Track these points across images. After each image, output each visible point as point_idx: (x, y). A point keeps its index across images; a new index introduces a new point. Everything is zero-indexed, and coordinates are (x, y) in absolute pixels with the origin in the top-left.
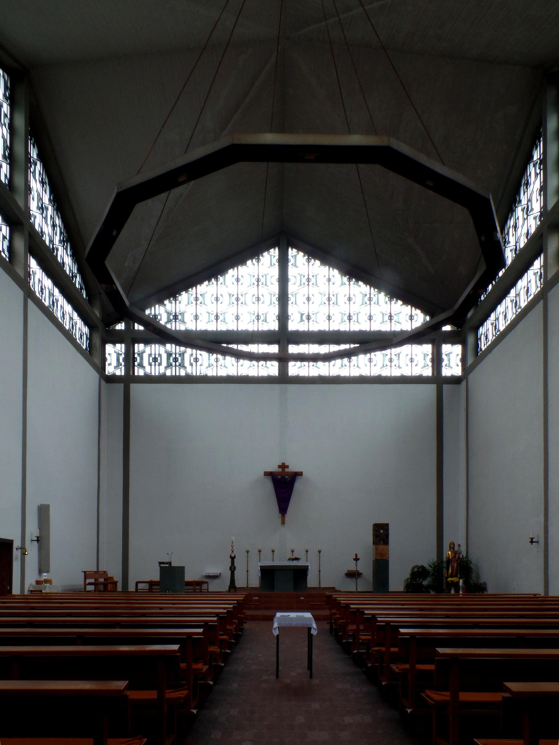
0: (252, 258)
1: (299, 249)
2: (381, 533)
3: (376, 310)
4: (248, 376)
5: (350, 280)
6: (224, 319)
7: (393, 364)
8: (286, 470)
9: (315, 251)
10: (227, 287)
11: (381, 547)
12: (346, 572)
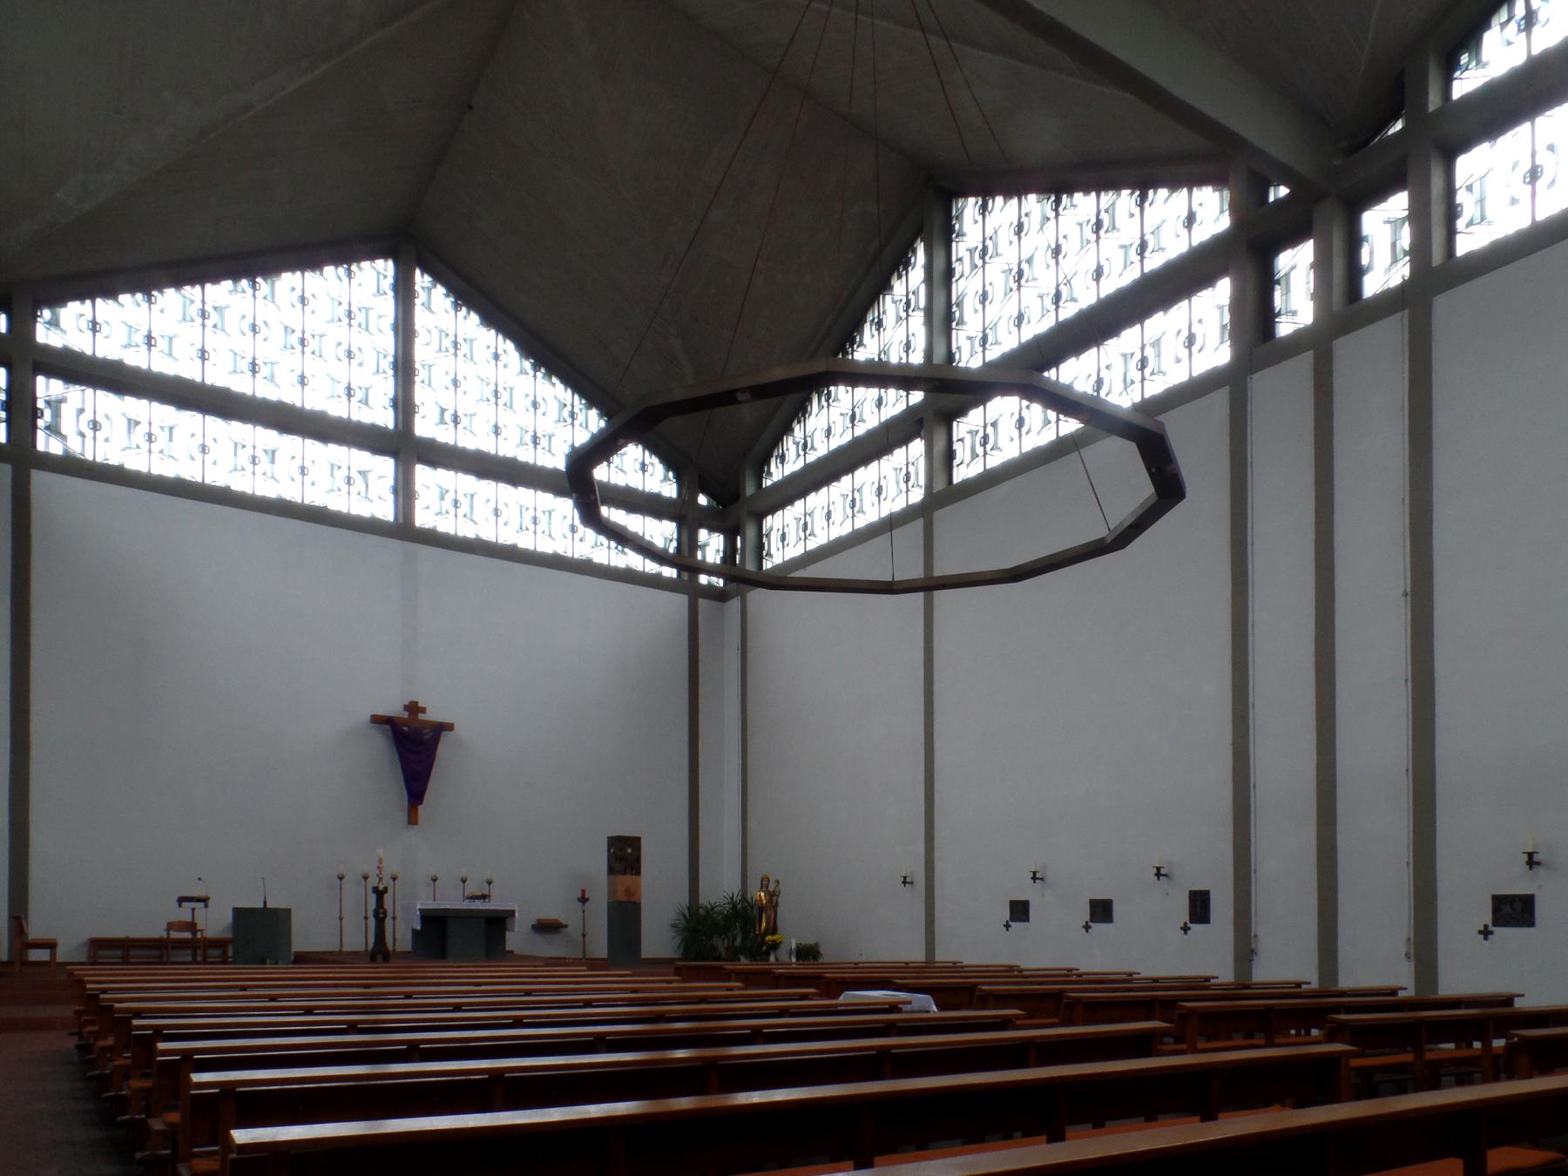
0: (337, 261)
1: (438, 278)
2: (624, 855)
3: (189, 336)
4: (325, 508)
5: (536, 367)
6: (273, 376)
7: (460, 512)
8: (421, 716)
9: (468, 293)
10: (278, 308)
11: (625, 880)
12: (534, 922)
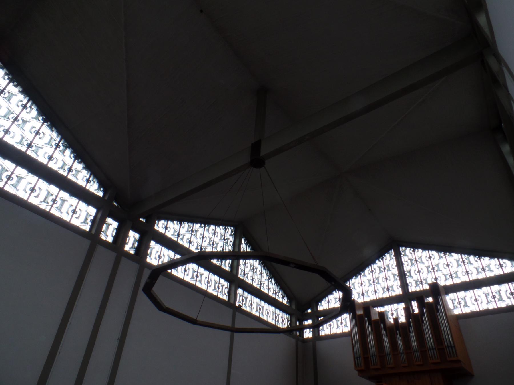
1: (406, 246)
3: (469, 267)
5: (445, 254)
